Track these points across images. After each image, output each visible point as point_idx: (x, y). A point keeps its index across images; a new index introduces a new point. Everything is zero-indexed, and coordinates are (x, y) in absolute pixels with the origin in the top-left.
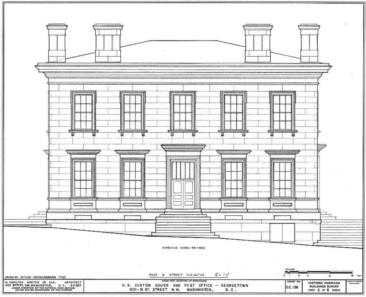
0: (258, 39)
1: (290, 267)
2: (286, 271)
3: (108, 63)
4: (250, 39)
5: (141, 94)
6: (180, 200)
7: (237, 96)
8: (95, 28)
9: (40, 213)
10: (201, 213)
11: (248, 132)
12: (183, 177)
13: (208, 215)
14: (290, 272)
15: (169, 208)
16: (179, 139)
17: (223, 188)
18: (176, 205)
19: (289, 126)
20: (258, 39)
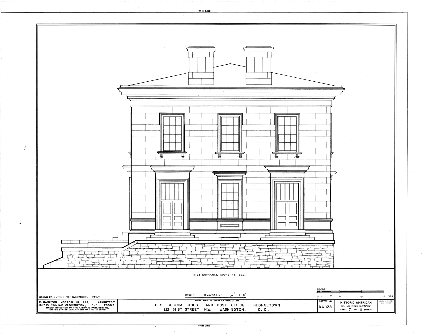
0: (259, 61)
3: (202, 87)
4: (251, 61)
5: (181, 116)
8: (245, 50)
10: (189, 234)
11: (302, 153)
12: (287, 198)
13: (312, 236)
15: (303, 229)
16: (284, 160)
17: (220, 209)
18: (166, 226)
19: (236, 148)
20: (201, 61)
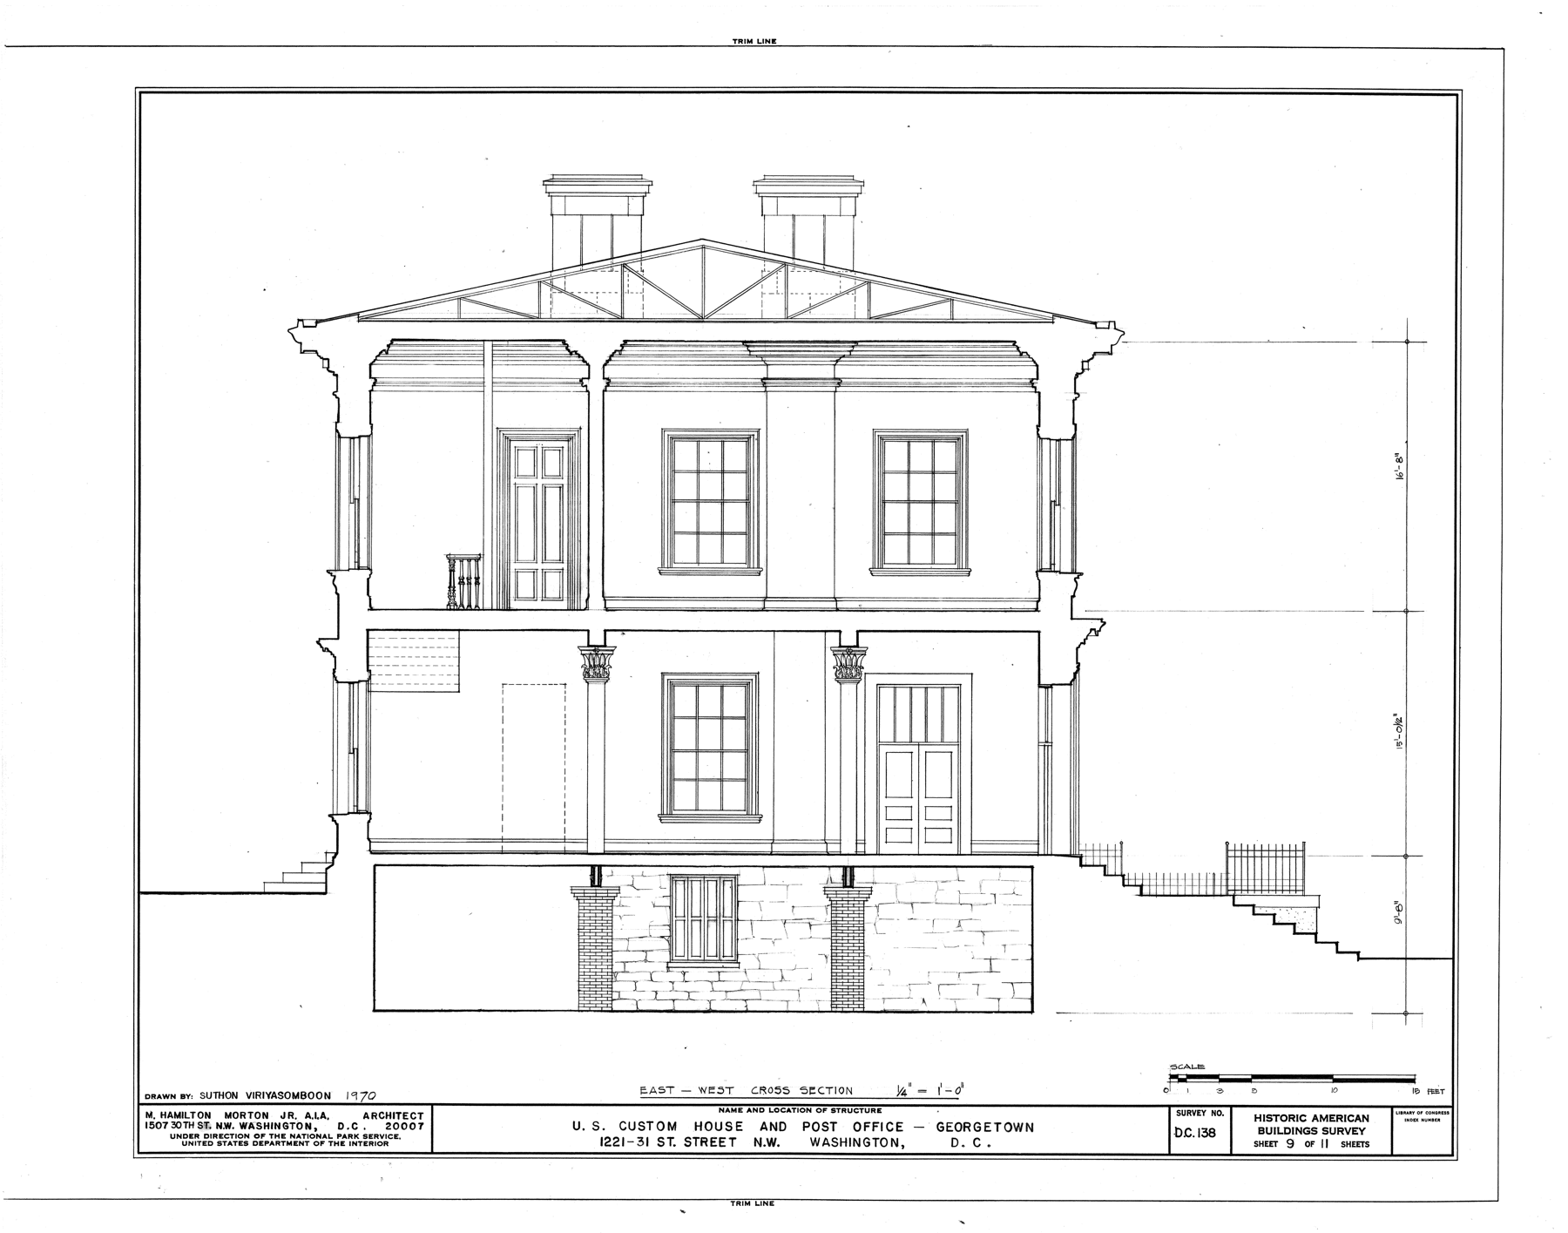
1: (1189, 1057)
2: (1174, 1072)
6: (908, 824)
7: (933, 442)
9: (307, 868)
14: (1190, 1076)
